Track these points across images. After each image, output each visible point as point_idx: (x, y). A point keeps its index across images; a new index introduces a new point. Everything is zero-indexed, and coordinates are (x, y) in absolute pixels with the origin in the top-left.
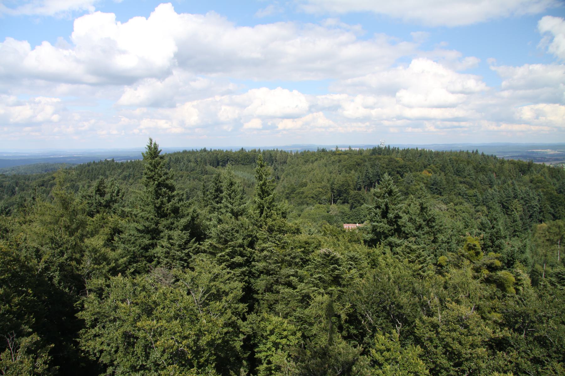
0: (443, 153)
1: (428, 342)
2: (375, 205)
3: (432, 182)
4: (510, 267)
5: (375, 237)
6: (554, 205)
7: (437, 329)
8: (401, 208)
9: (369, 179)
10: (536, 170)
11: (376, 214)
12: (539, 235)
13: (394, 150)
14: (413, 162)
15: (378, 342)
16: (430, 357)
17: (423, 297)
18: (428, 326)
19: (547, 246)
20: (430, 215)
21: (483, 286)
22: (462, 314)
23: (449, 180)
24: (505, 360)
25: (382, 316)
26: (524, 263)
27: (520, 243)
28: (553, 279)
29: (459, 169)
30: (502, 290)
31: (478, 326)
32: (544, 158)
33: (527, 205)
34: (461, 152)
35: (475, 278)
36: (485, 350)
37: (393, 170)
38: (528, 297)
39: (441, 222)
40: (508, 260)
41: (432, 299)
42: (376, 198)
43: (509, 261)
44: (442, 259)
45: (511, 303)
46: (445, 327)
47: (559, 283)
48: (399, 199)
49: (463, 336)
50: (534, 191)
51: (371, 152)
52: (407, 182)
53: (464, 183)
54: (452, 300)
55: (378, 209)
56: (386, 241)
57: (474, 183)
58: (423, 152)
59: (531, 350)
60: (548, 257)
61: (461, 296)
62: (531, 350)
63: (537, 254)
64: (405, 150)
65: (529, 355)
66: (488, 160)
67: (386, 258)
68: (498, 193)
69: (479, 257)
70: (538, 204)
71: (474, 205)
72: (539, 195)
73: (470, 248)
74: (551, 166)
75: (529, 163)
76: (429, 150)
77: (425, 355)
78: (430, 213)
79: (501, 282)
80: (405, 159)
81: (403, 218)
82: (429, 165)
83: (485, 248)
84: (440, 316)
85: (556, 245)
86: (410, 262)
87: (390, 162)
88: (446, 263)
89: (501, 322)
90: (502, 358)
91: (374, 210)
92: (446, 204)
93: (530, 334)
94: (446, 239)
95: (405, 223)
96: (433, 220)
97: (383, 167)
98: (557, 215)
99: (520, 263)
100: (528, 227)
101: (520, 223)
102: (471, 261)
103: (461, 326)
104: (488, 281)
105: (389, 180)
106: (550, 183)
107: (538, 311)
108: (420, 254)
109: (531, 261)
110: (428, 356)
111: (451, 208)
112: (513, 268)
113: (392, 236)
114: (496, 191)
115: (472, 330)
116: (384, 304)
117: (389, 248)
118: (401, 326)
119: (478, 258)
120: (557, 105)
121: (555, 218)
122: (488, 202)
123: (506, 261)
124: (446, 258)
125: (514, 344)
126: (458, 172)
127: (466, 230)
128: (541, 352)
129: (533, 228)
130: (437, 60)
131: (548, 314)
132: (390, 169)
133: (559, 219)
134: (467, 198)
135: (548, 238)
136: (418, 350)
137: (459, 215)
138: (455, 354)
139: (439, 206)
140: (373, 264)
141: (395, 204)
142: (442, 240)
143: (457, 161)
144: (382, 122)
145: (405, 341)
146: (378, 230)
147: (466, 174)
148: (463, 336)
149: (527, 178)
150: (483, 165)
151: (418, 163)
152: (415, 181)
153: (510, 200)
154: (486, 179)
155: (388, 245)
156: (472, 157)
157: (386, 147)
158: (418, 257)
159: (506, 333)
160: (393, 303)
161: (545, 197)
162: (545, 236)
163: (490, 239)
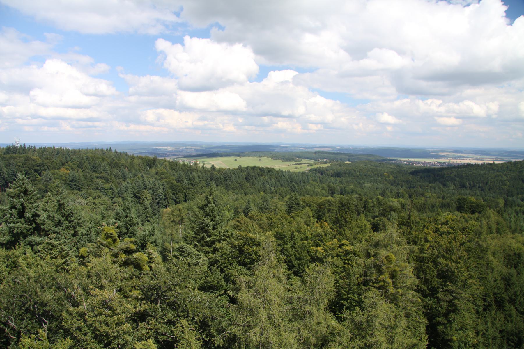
0: (80, 151)
1: (77, 331)
2: (9, 206)
3: (71, 179)
4: (143, 249)
5: (13, 239)
6: (175, 192)
7: (84, 317)
8: (38, 207)
9: (4, 179)
10: (160, 164)
11: (12, 215)
12: (166, 218)
13: (30, 148)
14: (51, 160)
15: (24, 347)
16: (81, 345)
17: (67, 290)
18: (75, 316)
19: (172, 226)
20: (68, 210)
21: (122, 269)
22: (105, 298)
23: (87, 175)
24: (147, 329)
25: (27, 318)
26: (154, 244)
27: (150, 227)
28: (177, 253)
29: (95, 166)
30: (139, 270)
31: (121, 305)
32: (165, 154)
33: (155, 194)
34: (96, 149)
35: (114, 263)
36: (129, 325)
37: (30, 169)
38: (159, 272)
39: (79, 216)
40: (141, 243)
41: (76, 290)
42: (10, 199)
43: (142, 244)
44: (83, 251)
45: (147, 279)
46: (92, 314)
47: (181, 255)
48: (36, 197)
49: (109, 318)
50: (159, 181)
51: (4, 151)
52: (45, 180)
53: (101, 178)
54: (96, 287)
55: (13, 210)
56: (25, 241)
57: (110, 177)
58: (60, 150)
59: (165, 315)
60: (174, 236)
61: (105, 282)
62: (165, 315)
63: (165, 234)
64: (41, 148)
65: (164, 320)
66: (120, 156)
67: (27, 258)
68: (131, 185)
69: (116, 243)
70: (163, 192)
71: (111, 197)
72: (163, 185)
73: (107, 237)
74: (171, 160)
75: (154, 158)
76: (66, 148)
77: (76, 344)
78: (68, 208)
79: (137, 262)
80: (42, 158)
81: (42, 216)
82: (67, 162)
83: (121, 235)
84: (85, 304)
85: (178, 225)
86: (52, 258)
87: (26, 160)
88: (87, 254)
89: (141, 297)
90: (143, 328)
91: (10, 211)
92: (86, 199)
93: (164, 302)
94: (85, 232)
95: (44, 221)
96: (71, 214)
97: (20, 166)
98: (178, 200)
99: (151, 244)
100: (157, 212)
101: (150, 209)
102: (110, 248)
103: (106, 308)
104: (126, 264)
105: (23, 179)
106: (170, 174)
107: (167, 281)
108: (62, 249)
109: (160, 241)
110: (79, 345)
111: (90, 202)
112: (146, 249)
113: (31, 235)
114: (129, 184)
115: (116, 310)
116: (26, 306)
117: (30, 248)
118: (48, 323)
119: (115, 245)
120: (172, 110)
121: (177, 203)
122: (122, 194)
123: (140, 245)
124: (87, 249)
125: (153, 314)
126: (94, 168)
127: (103, 220)
128: (172, 314)
129: (160, 213)
130: (71, 63)
131: (175, 282)
132: (27, 168)
133: (180, 203)
134: (104, 192)
135: (172, 220)
136: (68, 342)
137: (98, 207)
138: (103, 336)
139: (78, 201)
140: (13, 266)
141: (32, 203)
142: (82, 233)
143: (93, 158)
144: (16, 120)
145: (55, 337)
146: (15, 231)
147: (101, 169)
148: (109, 318)
149: (153, 171)
150: (116, 161)
151: (55, 161)
152: (53, 178)
153: (141, 190)
154: (120, 173)
155: (28, 245)
156: (107, 154)
157: (21, 146)
158: (60, 252)
159: (145, 306)
160: (36, 303)
161: (168, 186)
162: (170, 219)
163: (125, 227)
